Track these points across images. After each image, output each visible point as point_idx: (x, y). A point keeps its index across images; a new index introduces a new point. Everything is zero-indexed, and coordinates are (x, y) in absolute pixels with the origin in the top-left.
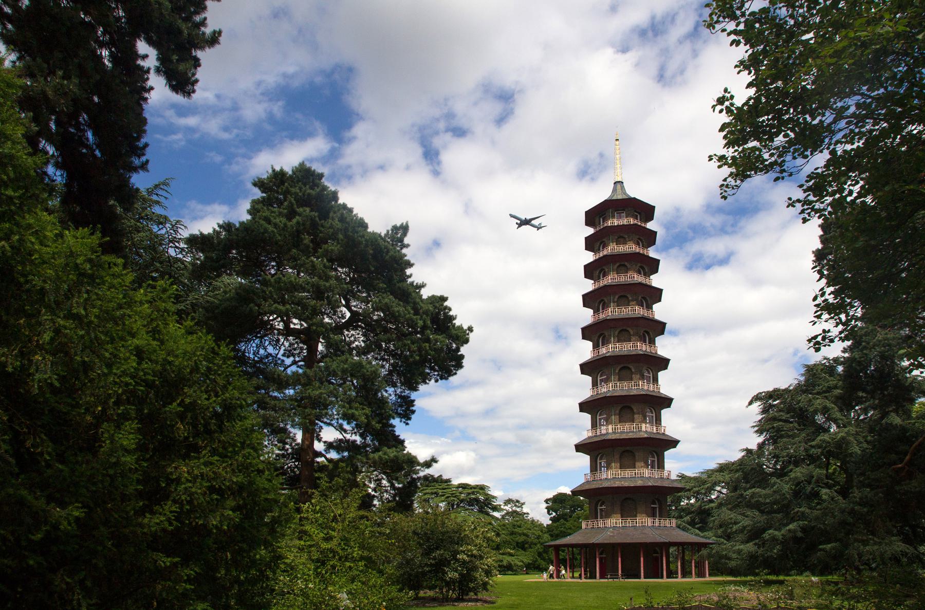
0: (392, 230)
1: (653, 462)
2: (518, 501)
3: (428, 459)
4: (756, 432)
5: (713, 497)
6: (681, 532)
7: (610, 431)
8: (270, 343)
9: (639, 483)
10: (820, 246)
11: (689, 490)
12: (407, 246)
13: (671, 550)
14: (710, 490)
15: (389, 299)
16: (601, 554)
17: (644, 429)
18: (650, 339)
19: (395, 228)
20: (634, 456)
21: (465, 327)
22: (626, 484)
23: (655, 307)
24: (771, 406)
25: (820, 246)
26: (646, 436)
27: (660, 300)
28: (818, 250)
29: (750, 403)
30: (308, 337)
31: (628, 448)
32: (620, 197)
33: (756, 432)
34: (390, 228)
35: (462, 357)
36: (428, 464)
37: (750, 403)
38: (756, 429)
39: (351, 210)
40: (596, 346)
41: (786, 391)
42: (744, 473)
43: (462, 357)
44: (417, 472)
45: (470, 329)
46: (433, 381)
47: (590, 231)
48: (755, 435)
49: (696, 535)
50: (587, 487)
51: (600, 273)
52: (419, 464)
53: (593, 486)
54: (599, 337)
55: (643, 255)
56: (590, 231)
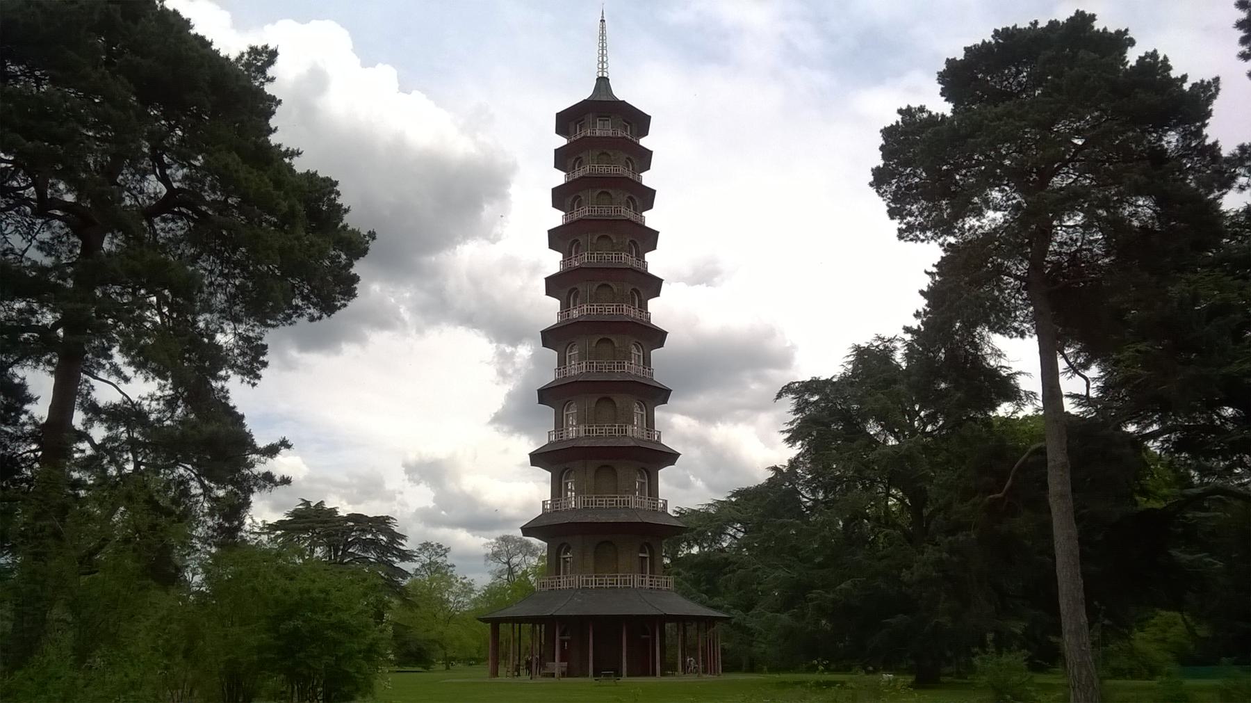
0: (249, 53)
1: (642, 484)
2: (440, 546)
3: (276, 441)
4: (788, 440)
5: (725, 545)
6: (681, 600)
7: (582, 434)
8: (16, 230)
9: (623, 518)
10: (881, 163)
11: (693, 530)
12: (272, 80)
13: (668, 625)
14: (720, 532)
15: (233, 159)
16: (562, 634)
17: (629, 433)
18: (640, 301)
19: (254, 51)
20: (616, 475)
21: (364, 232)
22: (603, 519)
23: (649, 257)
24: (807, 403)
25: (881, 163)
26: (632, 444)
27: (654, 248)
28: (878, 168)
29: (779, 396)
30: (85, 224)
31: (606, 462)
32: (604, 98)
33: (788, 440)
34: (246, 49)
35: (356, 279)
36: (272, 451)
37: (779, 396)
38: (787, 435)
39: (187, 24)
40: (565, 307)
41: (827, 382)
42: (764, 504)
43: (356, 279)
44: (252, 465)
45: (372, 235)
46: (306, 318)
47: (562, 141)
48: (786, 445)
49: (702, 603)
50: (545, 522)
51: (574, 201)
52: (256, 451)
53: (556, 521)
54: (570, 292)
55: (633, 181)
56: (562, 141)
